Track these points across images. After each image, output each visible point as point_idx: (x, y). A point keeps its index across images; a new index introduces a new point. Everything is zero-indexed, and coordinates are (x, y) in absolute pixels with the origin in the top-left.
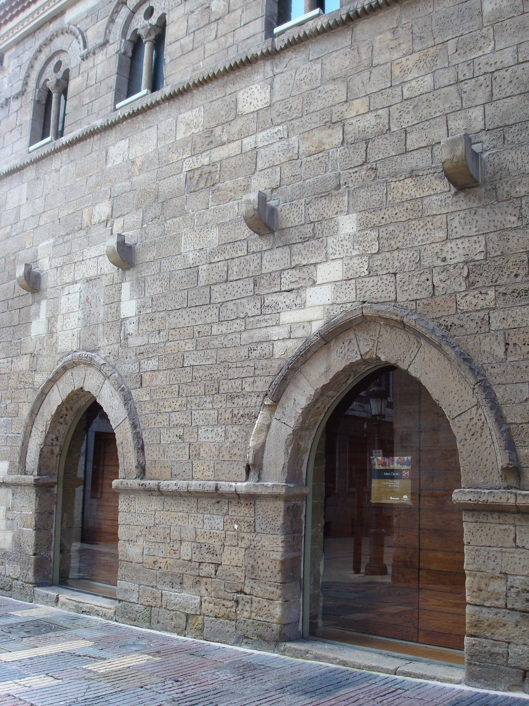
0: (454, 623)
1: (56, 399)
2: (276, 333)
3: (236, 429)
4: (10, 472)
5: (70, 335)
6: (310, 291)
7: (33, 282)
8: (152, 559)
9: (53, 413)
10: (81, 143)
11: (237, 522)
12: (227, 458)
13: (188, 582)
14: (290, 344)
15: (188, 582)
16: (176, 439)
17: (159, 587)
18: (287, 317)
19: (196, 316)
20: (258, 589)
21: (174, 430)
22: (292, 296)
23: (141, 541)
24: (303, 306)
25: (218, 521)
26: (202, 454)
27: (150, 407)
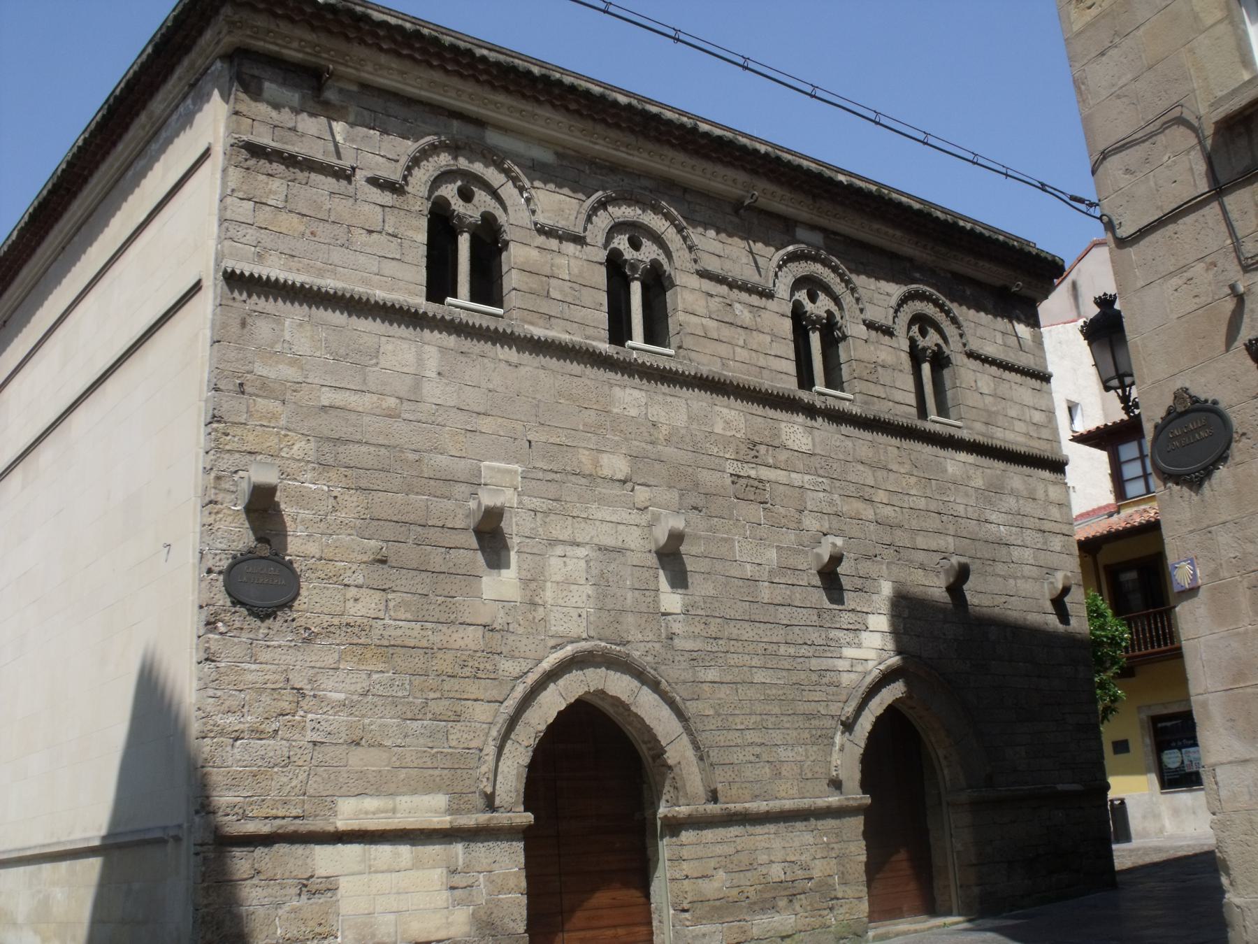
0: (768, 700)
1: (552, 703)
2: (842, 665)
3: (815, 748)
4: (451, 811)
5: (575, 615)
6: (864, 635)
7: (491, 536)
8: (737, 890)
9: (550, 721)
10: (665, 388)
11: (825, 835)
12: (809, 775)
13: (782, 903)
14: (853, 676)
15: (782, 903)
16: (752, 758)
17: (748, 918)
18: (849, 652)
19: (760, 632)
20: (849, 892)
21: (750, 748)
22: (851, 635)
23: (721, 874)
24: (859, 646)
25: (808, 838)
26: (784, 773)
27: (713, 724)
